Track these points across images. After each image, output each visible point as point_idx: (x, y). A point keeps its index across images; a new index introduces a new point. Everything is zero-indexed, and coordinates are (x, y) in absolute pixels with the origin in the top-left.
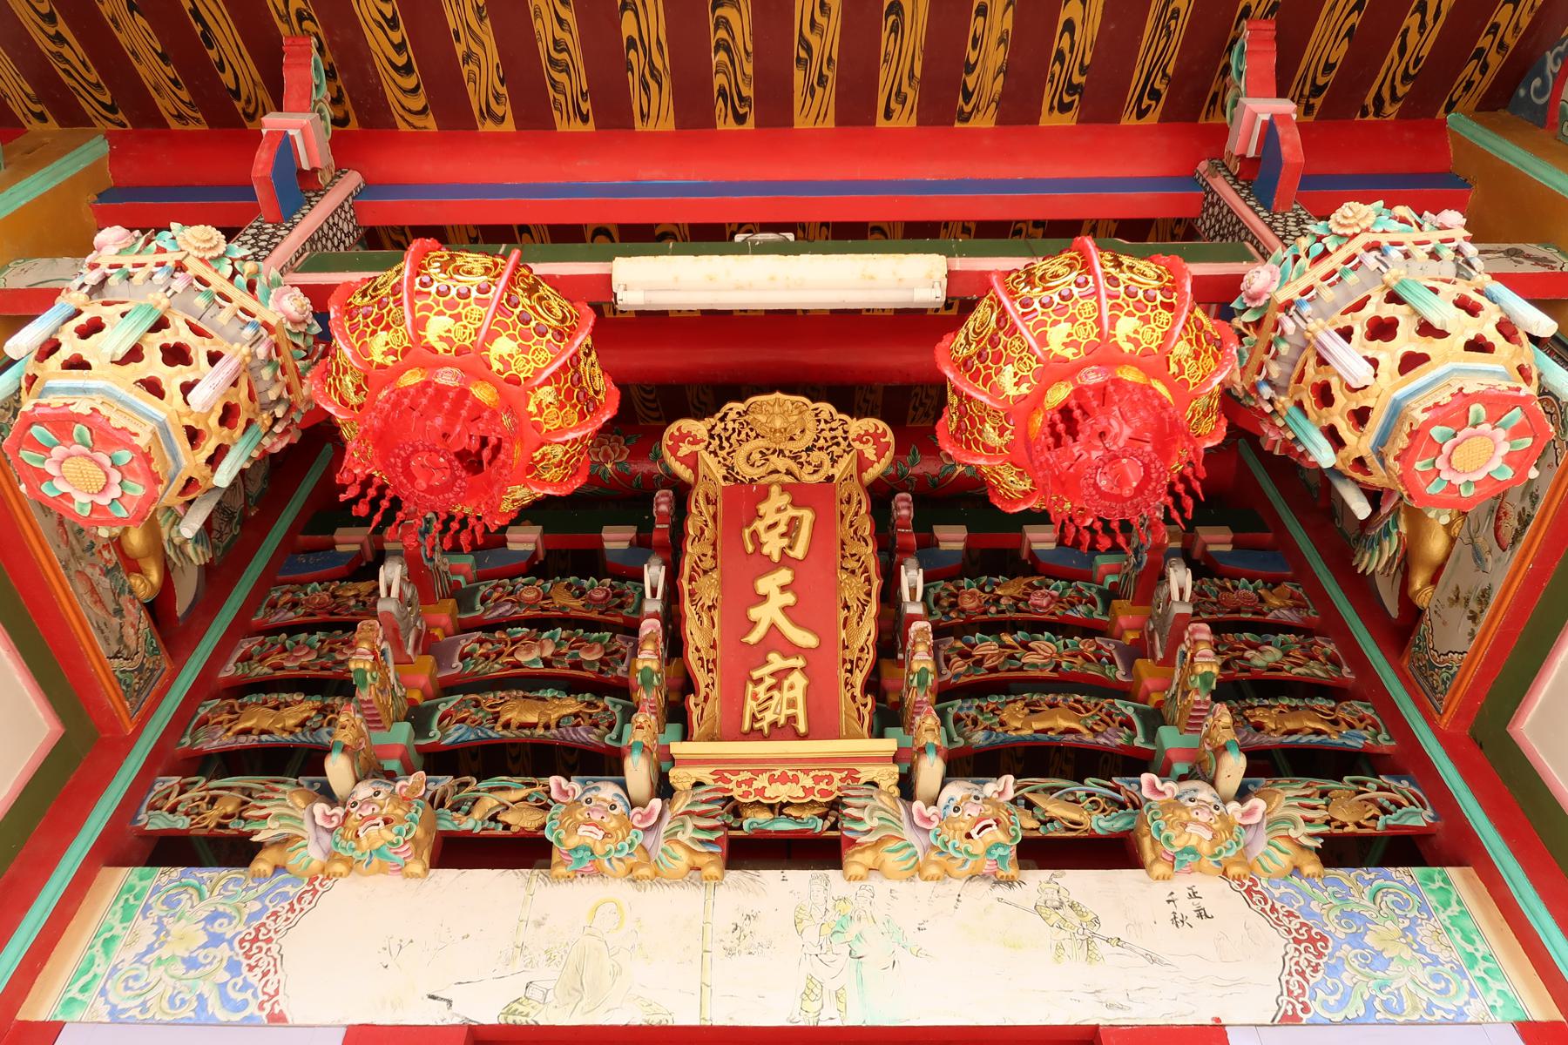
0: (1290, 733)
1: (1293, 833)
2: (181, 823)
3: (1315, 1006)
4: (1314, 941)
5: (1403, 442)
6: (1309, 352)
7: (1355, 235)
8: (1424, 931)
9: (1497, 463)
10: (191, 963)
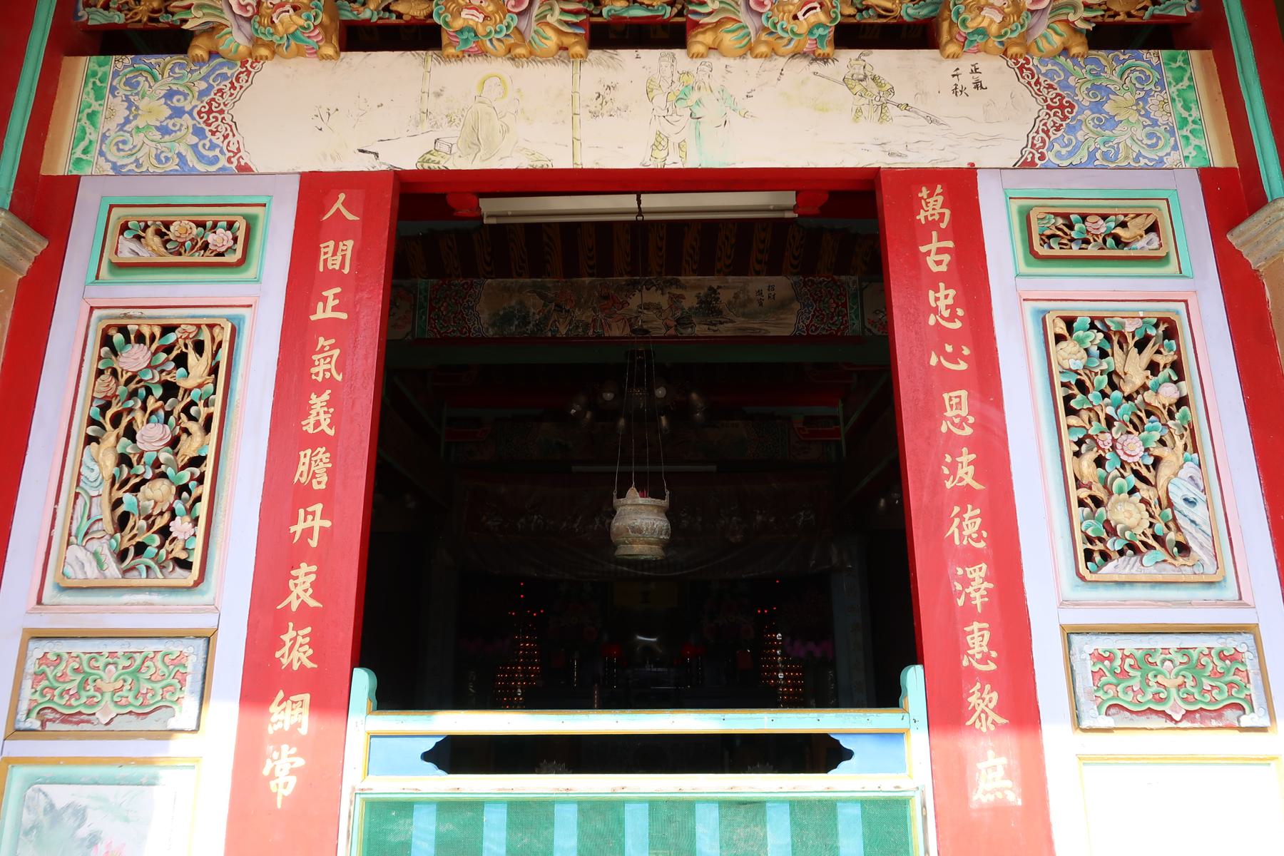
2: (119, 18)
4: (1062, 107)
10: (164, 130)
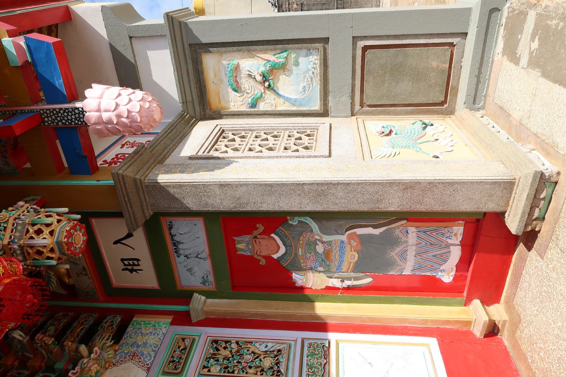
0: (78, 335)
1: (108, 345)
3: (148, 362)
4: (133, 356)
5: (66, 247)
6: (25, 248)
7: (8, 220)
8: (144, 331)
9: (82, 238)
